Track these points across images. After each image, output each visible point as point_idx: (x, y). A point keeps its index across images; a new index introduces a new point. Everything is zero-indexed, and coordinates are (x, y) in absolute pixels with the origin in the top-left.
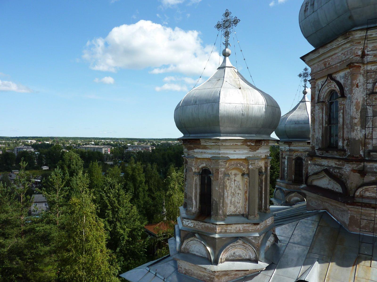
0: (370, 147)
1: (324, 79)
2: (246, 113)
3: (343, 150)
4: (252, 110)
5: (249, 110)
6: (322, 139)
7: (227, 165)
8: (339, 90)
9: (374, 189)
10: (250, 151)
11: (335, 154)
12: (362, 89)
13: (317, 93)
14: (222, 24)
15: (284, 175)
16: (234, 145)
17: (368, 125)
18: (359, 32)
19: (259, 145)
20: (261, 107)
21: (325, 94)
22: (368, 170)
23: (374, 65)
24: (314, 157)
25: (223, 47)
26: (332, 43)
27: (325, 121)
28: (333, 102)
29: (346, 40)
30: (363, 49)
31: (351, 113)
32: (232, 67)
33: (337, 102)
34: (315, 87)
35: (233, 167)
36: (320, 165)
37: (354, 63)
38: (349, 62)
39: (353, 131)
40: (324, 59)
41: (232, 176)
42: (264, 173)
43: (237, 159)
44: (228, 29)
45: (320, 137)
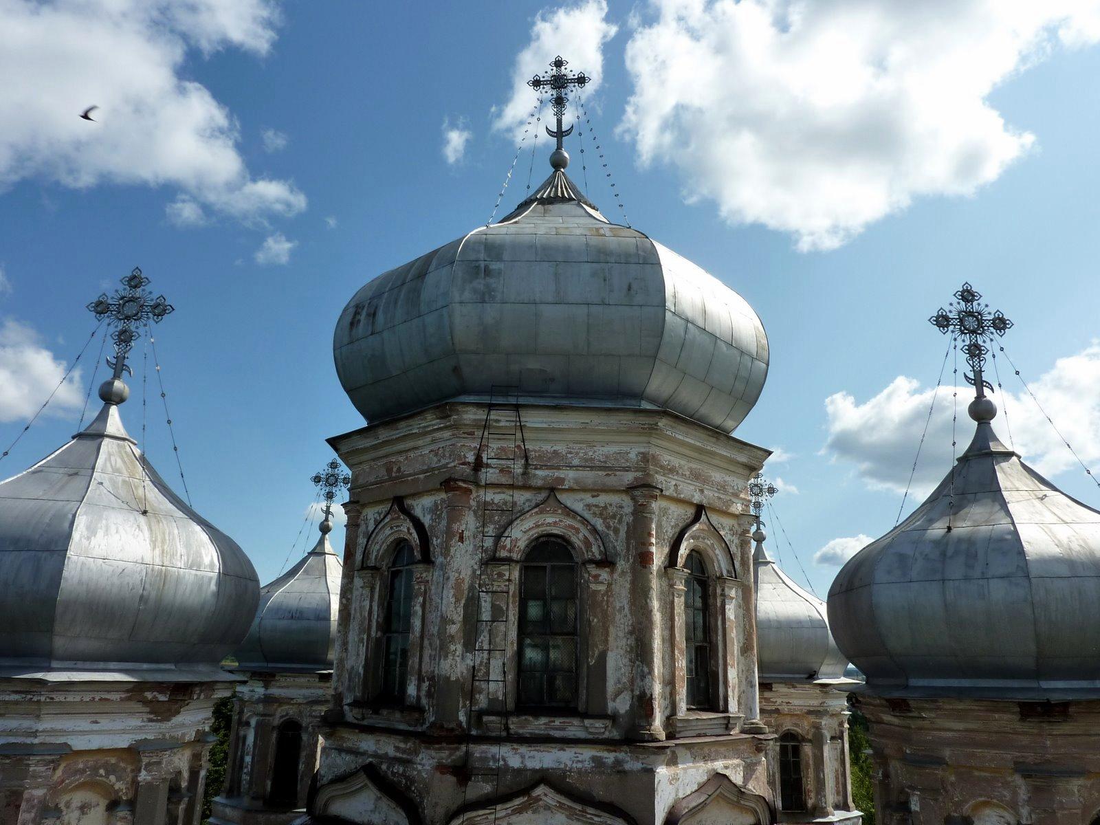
0: (482, 701)
1: (384, 508)
2: (153, 594)
3: (418, 709)
4: (177, 585)
5: (166, 587)
6: (364, 674)
7: (59, 773)
8: (418, 541)
9: (487, 818)
10: (150, 720)
11: (398, 720)
12: (472, 546)
13: (361, 541)
14: (115, 305)
15: (240, 781)
16: (97, 699)
17: (480, 640)
18: (472, 409)
19: (181, 700)
20: (206, 580)
21: (381, 546)
22: (477, 765)
23: (499, 493)
24: (338, 728)
25: (109, 373)
26: (411, 422)
27: (377, 622)
28: (400, 571)
29: (443, 421)
30: (479, 449)
31: (444, 609)
32: (124, 439)
33: (410, 573)
34: (358, 526)
35: (78, 780)
36: (355, 752)
37: (457, 480)
38: (447, 476)
39: (446, 657)
40: (386, 456)
41: (71, 815)
42: (184, 791)
43: (100, 751)
44: (132, 326)
45: (361, 668)
